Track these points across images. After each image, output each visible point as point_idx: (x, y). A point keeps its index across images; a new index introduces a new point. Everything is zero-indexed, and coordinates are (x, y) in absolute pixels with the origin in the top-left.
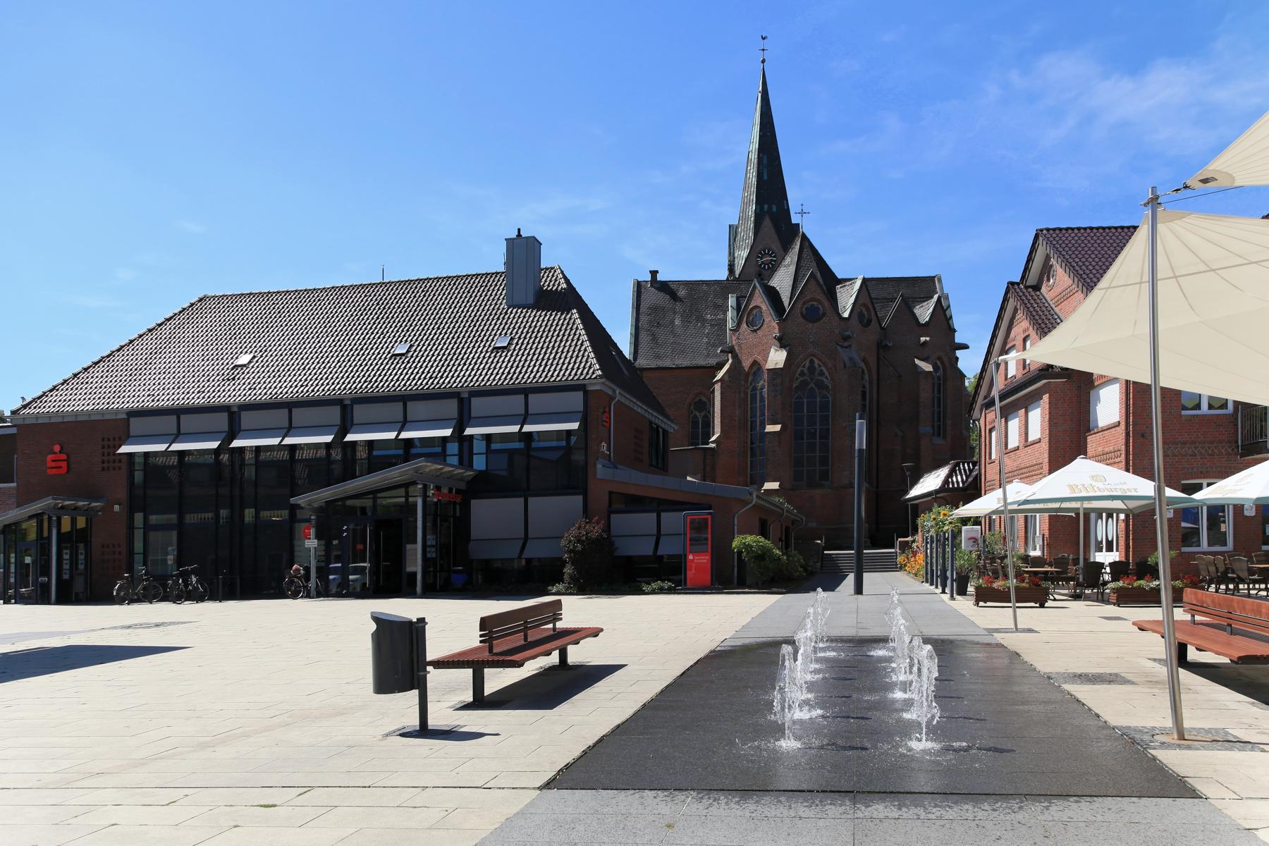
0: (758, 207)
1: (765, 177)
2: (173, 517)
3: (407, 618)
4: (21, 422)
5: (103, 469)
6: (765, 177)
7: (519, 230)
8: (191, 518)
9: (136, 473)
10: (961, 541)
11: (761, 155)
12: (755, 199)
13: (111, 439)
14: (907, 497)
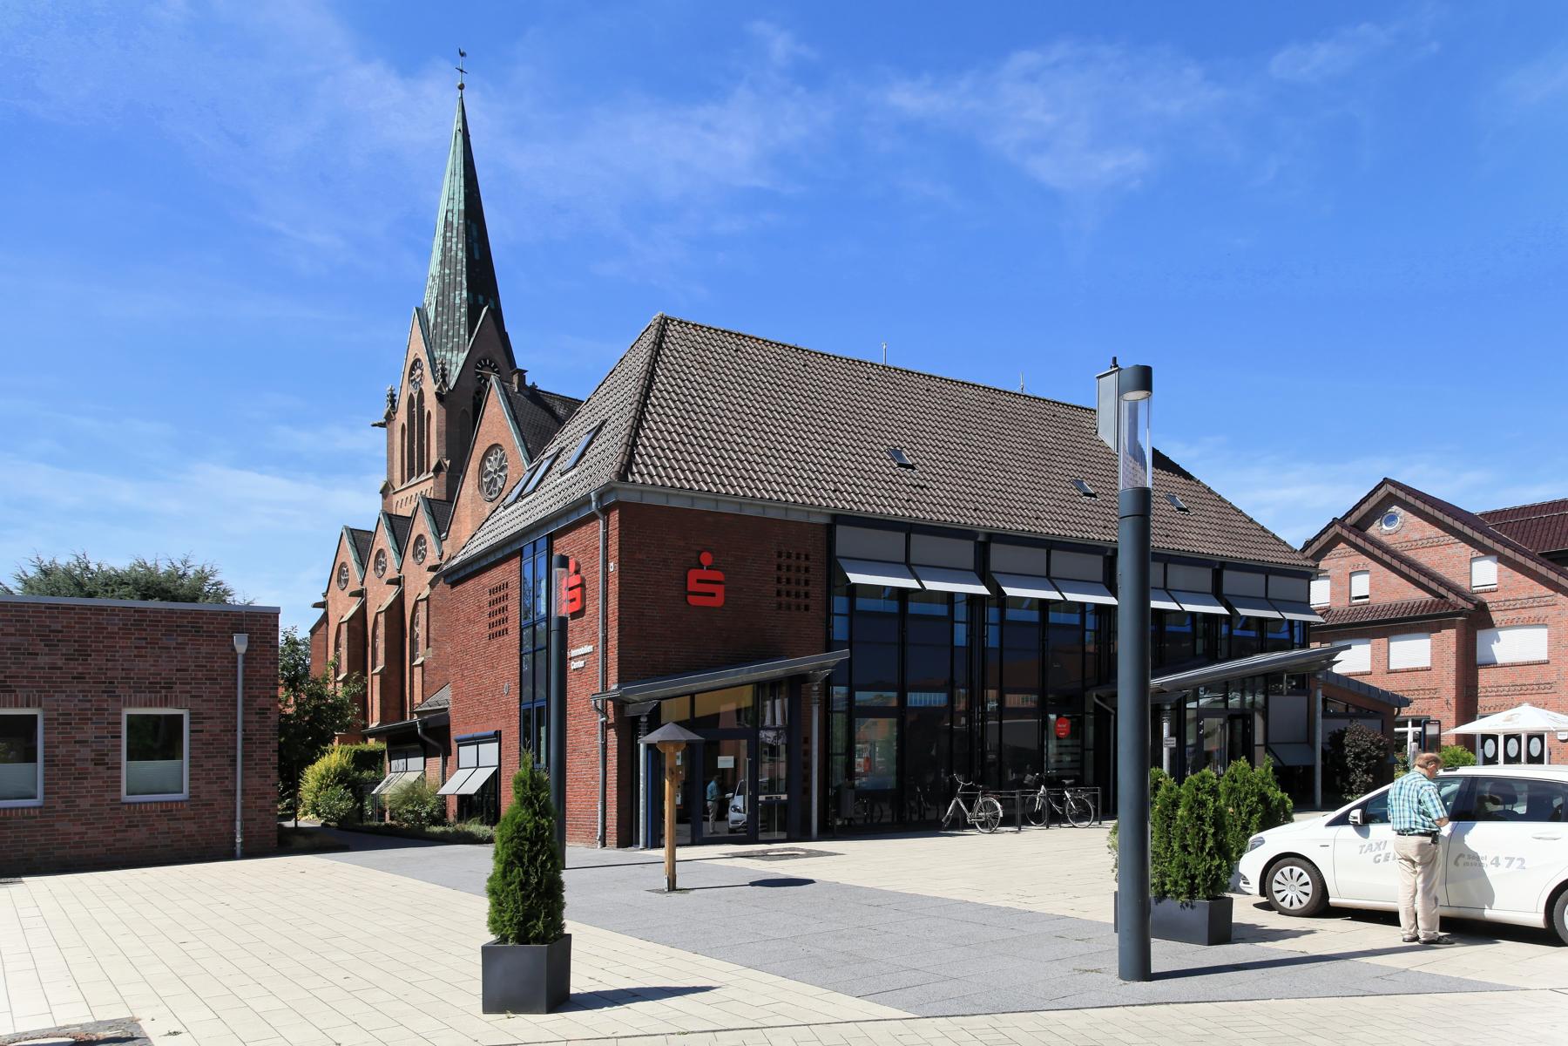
0: (471, 295)
1: (477, 256)
2: (892, 698)
3: (766, 874)
4: (634, 498)
5: (780, 606)
6: (477, 256)
7: (1115, 359)
8: (916, 699)
9: (1087, 633)
10: (1350, 801)
11: (469, 222)
12: (465, 282)
13: (794, 556)
14: (697, 737)
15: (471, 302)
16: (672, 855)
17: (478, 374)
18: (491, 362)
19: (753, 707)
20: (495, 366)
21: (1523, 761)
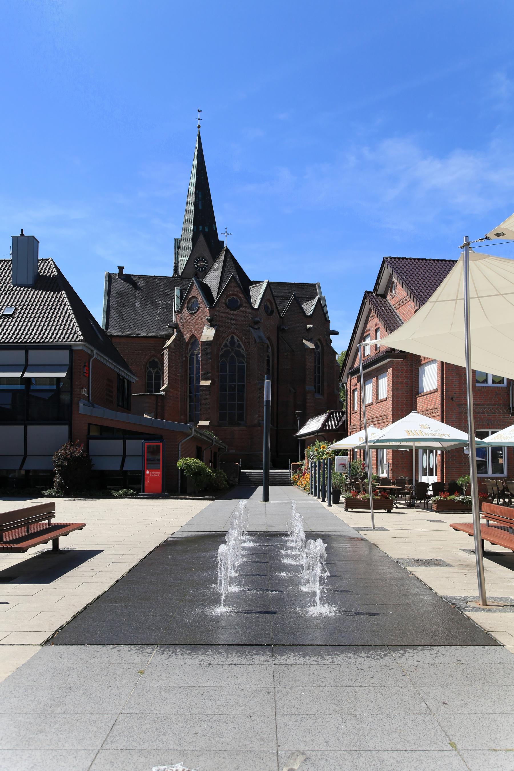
0: (195, 227)
1: (200, 207)
6: (200, 207)
11: (197, 192)
12: (193, 221)
15: (195, 230)
16: (267, 473)
17: (206, 263)
18: (202, 259)
19: (507, 387)
20: (205, 260)
21: (506, 448)
